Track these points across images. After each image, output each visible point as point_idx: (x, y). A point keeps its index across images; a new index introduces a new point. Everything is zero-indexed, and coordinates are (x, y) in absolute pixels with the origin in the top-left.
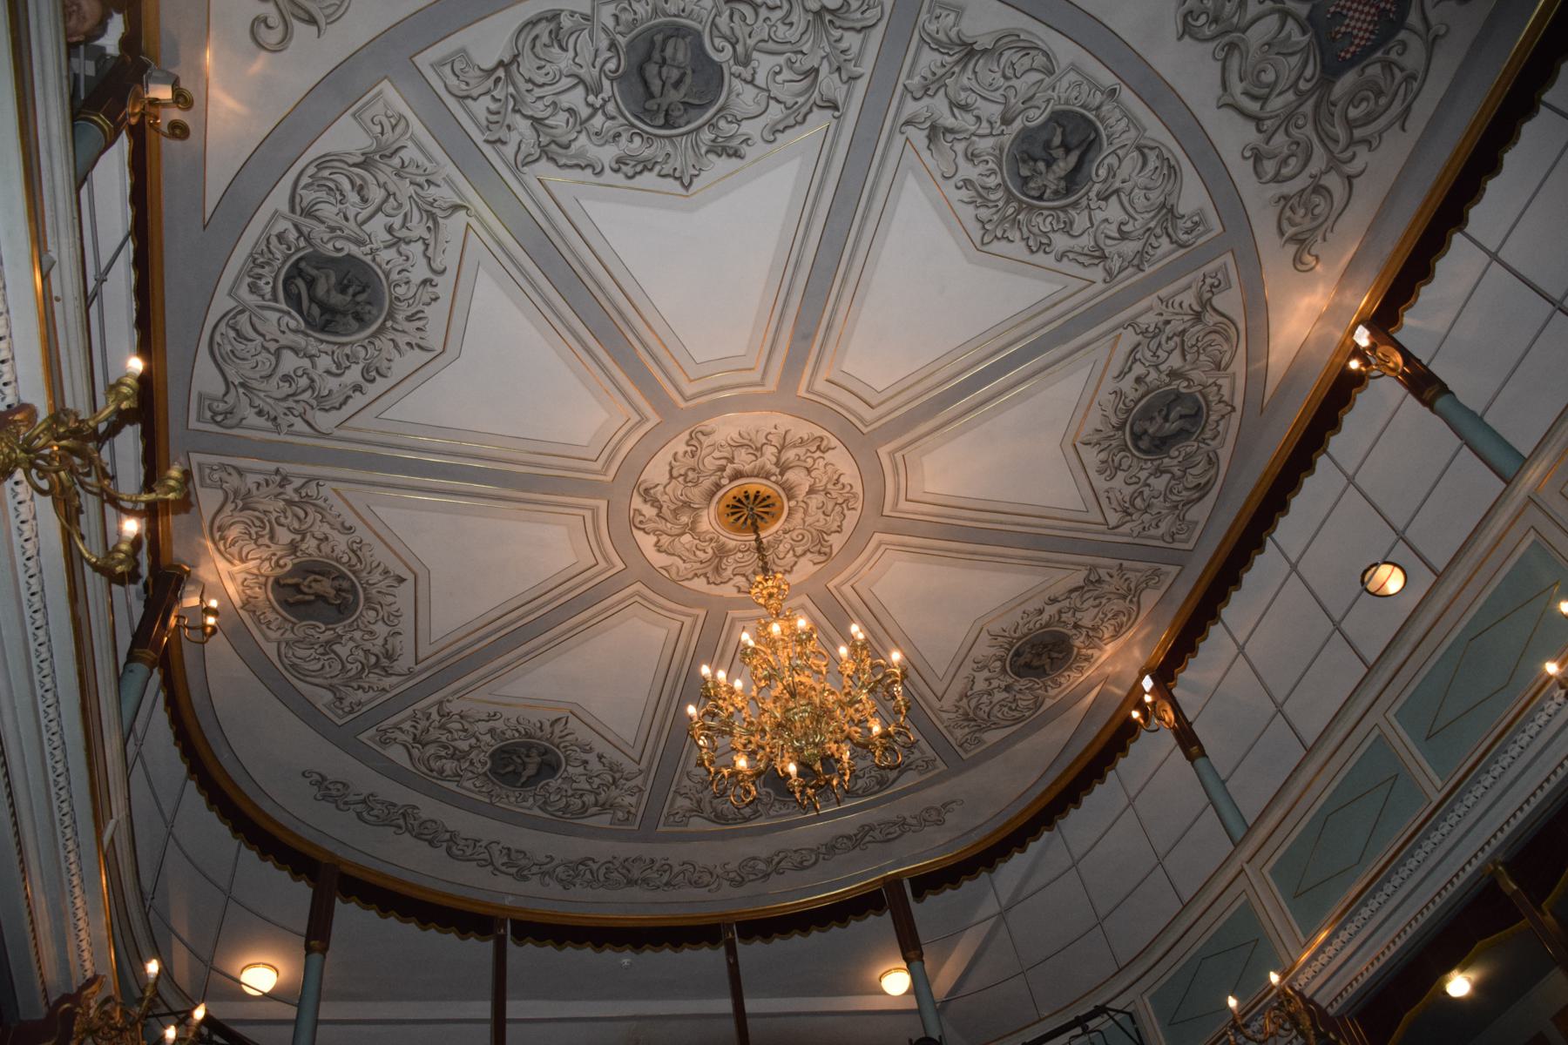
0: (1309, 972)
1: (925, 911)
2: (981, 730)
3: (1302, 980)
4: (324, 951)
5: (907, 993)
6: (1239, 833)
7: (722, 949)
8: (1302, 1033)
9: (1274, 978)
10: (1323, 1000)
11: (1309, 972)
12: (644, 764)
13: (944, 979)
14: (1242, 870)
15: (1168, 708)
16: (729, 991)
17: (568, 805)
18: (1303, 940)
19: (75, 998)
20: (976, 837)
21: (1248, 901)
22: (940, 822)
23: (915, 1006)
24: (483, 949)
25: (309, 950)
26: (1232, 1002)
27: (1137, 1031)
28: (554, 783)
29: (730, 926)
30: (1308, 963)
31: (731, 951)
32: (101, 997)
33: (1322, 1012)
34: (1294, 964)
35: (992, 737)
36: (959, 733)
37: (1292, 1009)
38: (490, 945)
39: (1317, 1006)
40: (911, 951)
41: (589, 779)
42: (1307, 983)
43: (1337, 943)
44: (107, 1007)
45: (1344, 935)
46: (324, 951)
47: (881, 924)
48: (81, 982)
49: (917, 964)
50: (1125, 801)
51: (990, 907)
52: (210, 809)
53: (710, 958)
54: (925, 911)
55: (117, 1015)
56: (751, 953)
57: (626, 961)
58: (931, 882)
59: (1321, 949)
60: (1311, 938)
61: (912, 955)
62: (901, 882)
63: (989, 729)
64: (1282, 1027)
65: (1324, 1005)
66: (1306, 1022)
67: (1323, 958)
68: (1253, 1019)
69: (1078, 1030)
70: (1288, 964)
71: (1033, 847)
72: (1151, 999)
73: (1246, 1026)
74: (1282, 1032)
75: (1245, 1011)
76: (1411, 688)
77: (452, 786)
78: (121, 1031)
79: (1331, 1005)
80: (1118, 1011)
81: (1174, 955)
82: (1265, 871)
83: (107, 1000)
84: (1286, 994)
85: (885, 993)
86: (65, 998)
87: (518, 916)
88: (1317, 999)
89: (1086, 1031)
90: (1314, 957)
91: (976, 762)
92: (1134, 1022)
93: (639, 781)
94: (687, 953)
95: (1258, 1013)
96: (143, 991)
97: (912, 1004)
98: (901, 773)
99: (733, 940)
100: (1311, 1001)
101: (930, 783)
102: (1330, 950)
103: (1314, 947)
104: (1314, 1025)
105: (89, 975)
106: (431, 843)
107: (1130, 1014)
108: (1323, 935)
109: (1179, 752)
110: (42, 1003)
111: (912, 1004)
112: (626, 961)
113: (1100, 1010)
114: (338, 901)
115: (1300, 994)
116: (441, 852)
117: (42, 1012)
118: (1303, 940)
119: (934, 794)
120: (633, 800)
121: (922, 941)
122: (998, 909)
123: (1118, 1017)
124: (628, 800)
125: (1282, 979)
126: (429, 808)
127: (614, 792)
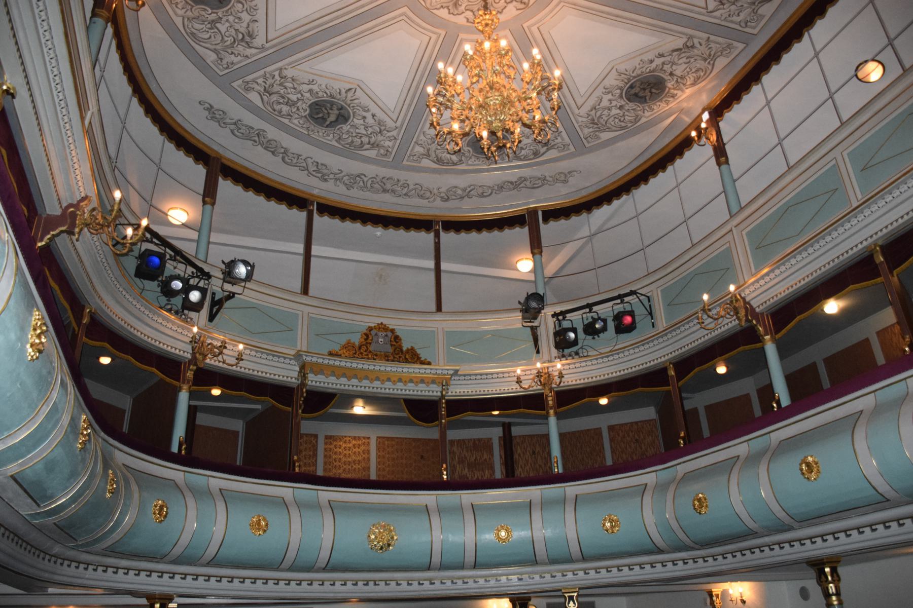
2: (600, 131)
12: (399, 124)
17: (352, 142)
20: (584, 193)
22: (565, 181)
28: (345, 127)
35: (605, 136)
36: (586, 131)
41: (366, 128)
45: (777, 272)
63: (604, 131)
71: (616, 203)
77: (286, 121)
91: (591, 150)
93: (394, 133)
100: (749, 303)
106: (273, 153)
109: (713, 159)
114: (220, 179)
115: (744, 299)
116: (279, 159)
119: (565, 165)
120: (390, 144)
124: (387, 143)
126: (272, 133)
127: (380, 138)
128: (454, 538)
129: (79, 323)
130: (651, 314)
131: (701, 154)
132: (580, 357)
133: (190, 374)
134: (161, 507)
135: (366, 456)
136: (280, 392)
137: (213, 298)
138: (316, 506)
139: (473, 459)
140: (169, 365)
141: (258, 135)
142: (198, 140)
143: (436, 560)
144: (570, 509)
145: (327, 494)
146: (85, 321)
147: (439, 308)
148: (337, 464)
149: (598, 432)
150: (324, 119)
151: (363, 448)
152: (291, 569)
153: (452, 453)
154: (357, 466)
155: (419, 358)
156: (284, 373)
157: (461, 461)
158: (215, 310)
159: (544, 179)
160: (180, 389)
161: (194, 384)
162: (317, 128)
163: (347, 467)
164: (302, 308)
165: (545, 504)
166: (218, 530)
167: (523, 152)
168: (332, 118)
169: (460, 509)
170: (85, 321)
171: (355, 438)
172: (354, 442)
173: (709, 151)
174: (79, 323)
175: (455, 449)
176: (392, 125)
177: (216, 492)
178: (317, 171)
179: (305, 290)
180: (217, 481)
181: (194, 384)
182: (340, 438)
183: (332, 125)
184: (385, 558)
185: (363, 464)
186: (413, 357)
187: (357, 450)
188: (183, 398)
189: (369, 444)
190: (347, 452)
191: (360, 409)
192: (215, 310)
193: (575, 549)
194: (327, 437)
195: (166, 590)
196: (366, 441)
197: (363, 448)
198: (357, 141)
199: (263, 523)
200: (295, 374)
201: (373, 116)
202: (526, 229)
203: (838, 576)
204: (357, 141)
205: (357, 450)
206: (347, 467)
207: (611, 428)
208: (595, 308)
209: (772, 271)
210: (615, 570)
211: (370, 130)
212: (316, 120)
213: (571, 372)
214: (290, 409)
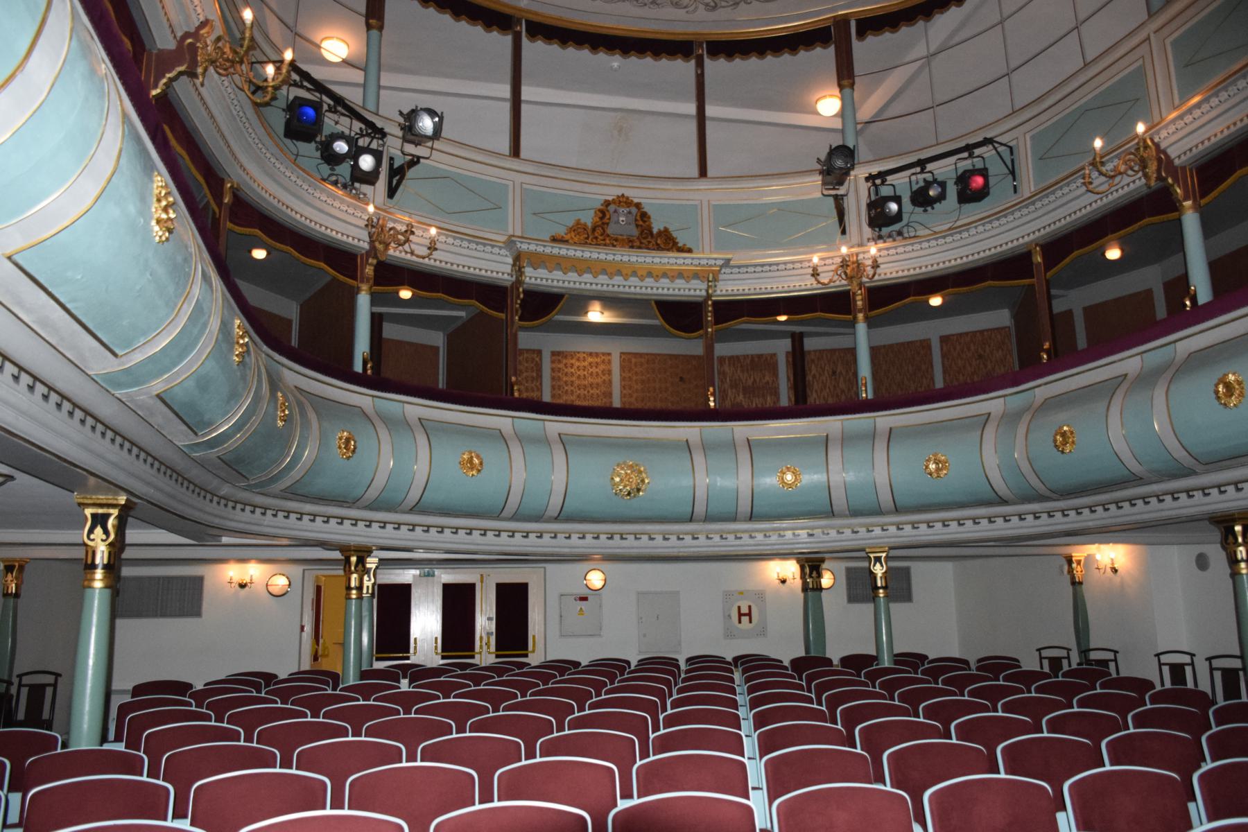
0: (1172, 129)
1: (864, 50)
3: (1164, 134)
4: (381, 28)
5: (835, 116)
7: (693, 62)
8: (1146, 175)
9: (1141, 128)
10: (1173, 153)
11: (1172, 129)
13: (866, 111)
14: (1148, 38)
16: (694, 99)
18: (1177, 102)
19: (195, 34)
21: (1143, 67)
23: (840, 127)
24: (504, 42)
25: (369, 27)
26: (1098, 143)
27: (1013, 161)
29: (700, 44)
30: (1173, 121)
31: (700, 64)
32: (213, 37)
33: (1169, 161)
34: (1162, 119)
37: (1145, 155)
38: (508, 39)
39: (1167, 156)
40: (845, 76)
42: (1165, 138)
43: (1205, 107)
44: (220, 44)
45: (1214, 101)
46: (381, 28)
47: (825, 56)
48: (197, 24)
49: (847, 91)
50: (997, 18)
51: (920, 50)
53: (682, 69)
54: (864, 50)
55: (227, 50)
56: (716, 68)
57: (615, 65)
58: (872, 24)
59: (1190, 111)
60: (1185, 97)
61: (845, 82)
64: (1131, 168)
65: (1173, 156)
66: (1152, 167)
67: (1188, 119)
68: (1111, 160)
69: (965, 155)
70: (1157, 119)
72: (1032, 138)
73: (1103, 164)
74: (1130, 172)
75: (1106, 153)
78: (233, 62)
79: (1179, 157)
80: (1001, 144)
82: (1168, 41)
83: (219, 39)
84: (1145, 141)
85: (818, 114)
86: (187, 35)
87: (531, 17)
88: (1169, 151)
89: (971, 156)
90: (1181, 117)
92: (1012, 153)
94: (664, 63)
95: (1116, 156)
96: (243, 33)
97: (838, 124)
99: (702, 56)
100: (1164, 152)
102: (1197, 113)
103: (1184, 108)
104: (1159, 171)
105: (202, 18)
107: (1011, 148)
108: (1196, 100)
110: (171, 37)
111: (838, 124)
112: (615, 65)
113: (987, 141)
115: (1157, 145)
118: (1177, 102)
121: (857, 71)
122: (925, 54)
123: (1001, 149)
125: (1146, 132)
128: (724, 482)
129: (219, 203)
130: (1013, 173)
133: (369, 270)
136: (489, 293)
137: (391, 165)
138: (543, 441)
139: (750, 382)
140: (341, 258)
143: (700, 509)
145: (556, 425)
147: (703, 172)
148: (569, 388)
149: (925, 345)
151: (602, 367)
152: (515, 517)
153: (723, 374)
156: (493, 266)
158: (395, 182)
160: (358, 290)
164: (511, 176)
166: (421, 468)
171: (591, 354)
172: (590, 360)
174: (219, 203)
175: (726, 368)
179: (515, 151)
180: (415, 408)
182: (572, 355)
185: (603, 389)
187: (594, 370)
188: (363, 301)
189: (610, 362)
190: (581, 373)
191: (596, 315)
192: (395, 182)
193: (885, 499)
194: (553, 354)
196: (606, 358)
205: (594, 370)
207: (944, 340)
214: (503, 316)
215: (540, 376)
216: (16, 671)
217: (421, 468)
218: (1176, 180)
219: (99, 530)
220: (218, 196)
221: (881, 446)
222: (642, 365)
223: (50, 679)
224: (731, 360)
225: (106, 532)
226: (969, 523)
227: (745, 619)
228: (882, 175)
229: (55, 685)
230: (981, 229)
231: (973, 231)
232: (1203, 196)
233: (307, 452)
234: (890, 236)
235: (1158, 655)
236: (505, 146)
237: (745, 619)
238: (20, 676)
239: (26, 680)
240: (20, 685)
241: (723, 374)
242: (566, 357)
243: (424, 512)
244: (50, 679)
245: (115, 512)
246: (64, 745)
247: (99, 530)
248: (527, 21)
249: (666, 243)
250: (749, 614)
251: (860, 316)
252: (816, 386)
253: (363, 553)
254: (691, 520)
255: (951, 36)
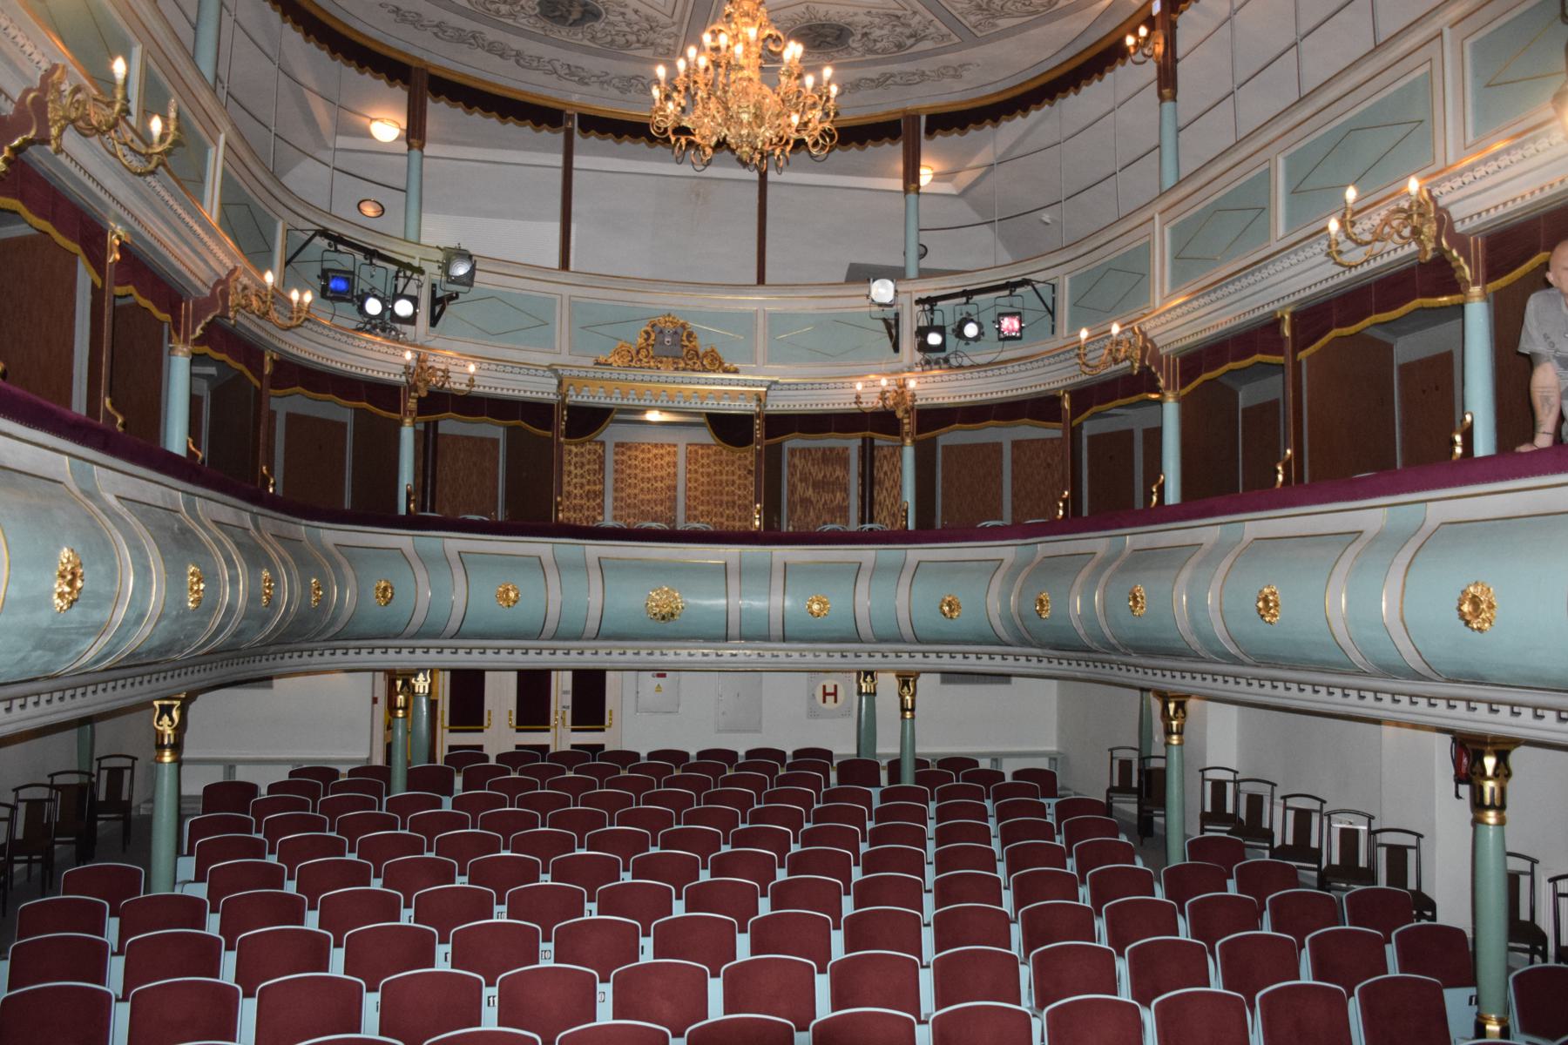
2: (994, 16)
6: (1169, 181)
12: (676, 18)
15: (1161, 41)
17: (613, 41)
20: (990, 90)
22: (957, 76)
28: (599, 26)
33: (1155, 349)
35: (1004, 23)
36: (973, 18)
38: (560, 137)
41: (629, 24)
43: (1185, 309)
45: (1195, 304)
52: (308, 41)
62: (919, 118)
63: (1002, 17)
71: (1034, 115)
76: (1302, 144)
77: (510, 21)
81: (1110, 247)
86: (219, 282)
91: (988, 39)
93: (674, 29)
98: (917, 41)
100: (1151, 341)
101: (945, 50)
106: (501, 56)
109: (1155, 85)
114: (430, 103)
115: (1144, 334)
116: (512, 61)
117: (207, 292)
119: (952, 58)
120: (671, 41)
124: (666, 41)
126: (491, 34)
127: (652, 36)
128: (758, 604)
129: (260, 376)
130: (1052, 313)
131: (1136, 75)
132: (951, 368)
133: (412, 404)
134: (385, 589)
135: (671, 470)
136: (537, 412)
137: (434, 293)
138: (583, 567)
139: (820, 476)
140: (384, 394)
141: (474, 37)
142: (389, 48)
143: (734, 631)
144: (905, 579)
145: (595, 550)
146: (268, 370)
147: (761, 279)
148: (633, 481)
149: (997, 448)
150: (566, 19)
151: (667, 459)
152: (554, 638)
153: (793, 466)
154: (659, 484)
155: (721, 364)
156: (541, 389)
157: (804, 479)
158: (438, 309)
159: (923, 73)
160: (400, 424)
161: (419, 414)
162: (556, 28)
163: (645, 485)
164: (562, 291)
165: (877, 570)
166: (458, 598)
167: (879, 45)
168: (576, 15)
169: (768, 571)
170: (268, 370)
171: (656, 446)
172: (655, 451)
173: (1150, 70)
174: (260, 376)
175: (797, 461)
176: (669, 21)
177: (454, 557)
178: (572, 74)
179: (565, 264)
180: (455, 543)
181: (419, 414)
182: (636, 446)
183: (575, 23)
184: (670, 626)
185: (668, 482)
186: (714, 362)
187: (659, 462)
188: (407, 434)
189: (675, 453)
190: (646, 465)
191: (653, 416)
192: (438, 309)
193: (906, 630)
194: (617, 445)
195: (407, 665)
196: (672, 449)
197: (667, 459)
198: (621, 40)
199: (512, 595)
200: (554, 389)
201: (636, 12)
202: (900, 147)
203: (1184, 712)
204: (621, 40)
205: (659, 462)
206: (645, 485)
207: (1016, 445)
208: (976, 298)
209: (1190, 301)
210: (960, 656)
211: (636, 28)
212: (553, 19)
213: (931, 388)
214: (549, 434)
215: (602, 469)
216: (96, 755)
217: (458, 598)
218: (1160, 368)
219: (166, 718)
220: (257, 369)
221: (905, 579)
222: (709, 456)
223: (128, 762)
224: (783, 472)
225: (171, 719)
226: (986, 657)
227: (830, 699)
228: (931, 301)
229: (132, 768)
230: (1010, 370)
231: (1010, 370)
232: (1183, 386)
233: (347, 597)
234: (937, 362)
235: (1203, 771)
236: (555, 261)
237: (830, 699)
238: (99, 760)
239: (105, 763)
240: (100, 768)
241: (793, 466)
242: (630, 449)
243: (465, 637)
244: (128, 762)
245: (178, 703)
246: (148, 889)
247: (166, 718)
248: (580, 116)
249: (712, 363)
250: (835, 694)
251: (908, 441)
252: (887, 484)
253: (408, 675)
254: (726, 639)
255: (1012, 147)
